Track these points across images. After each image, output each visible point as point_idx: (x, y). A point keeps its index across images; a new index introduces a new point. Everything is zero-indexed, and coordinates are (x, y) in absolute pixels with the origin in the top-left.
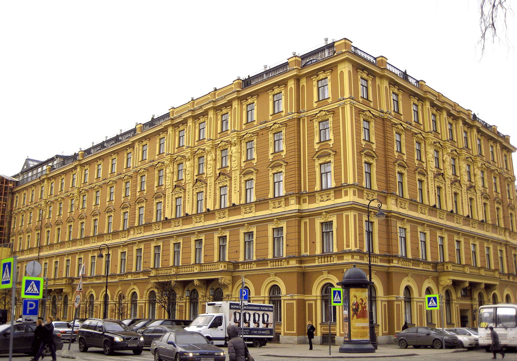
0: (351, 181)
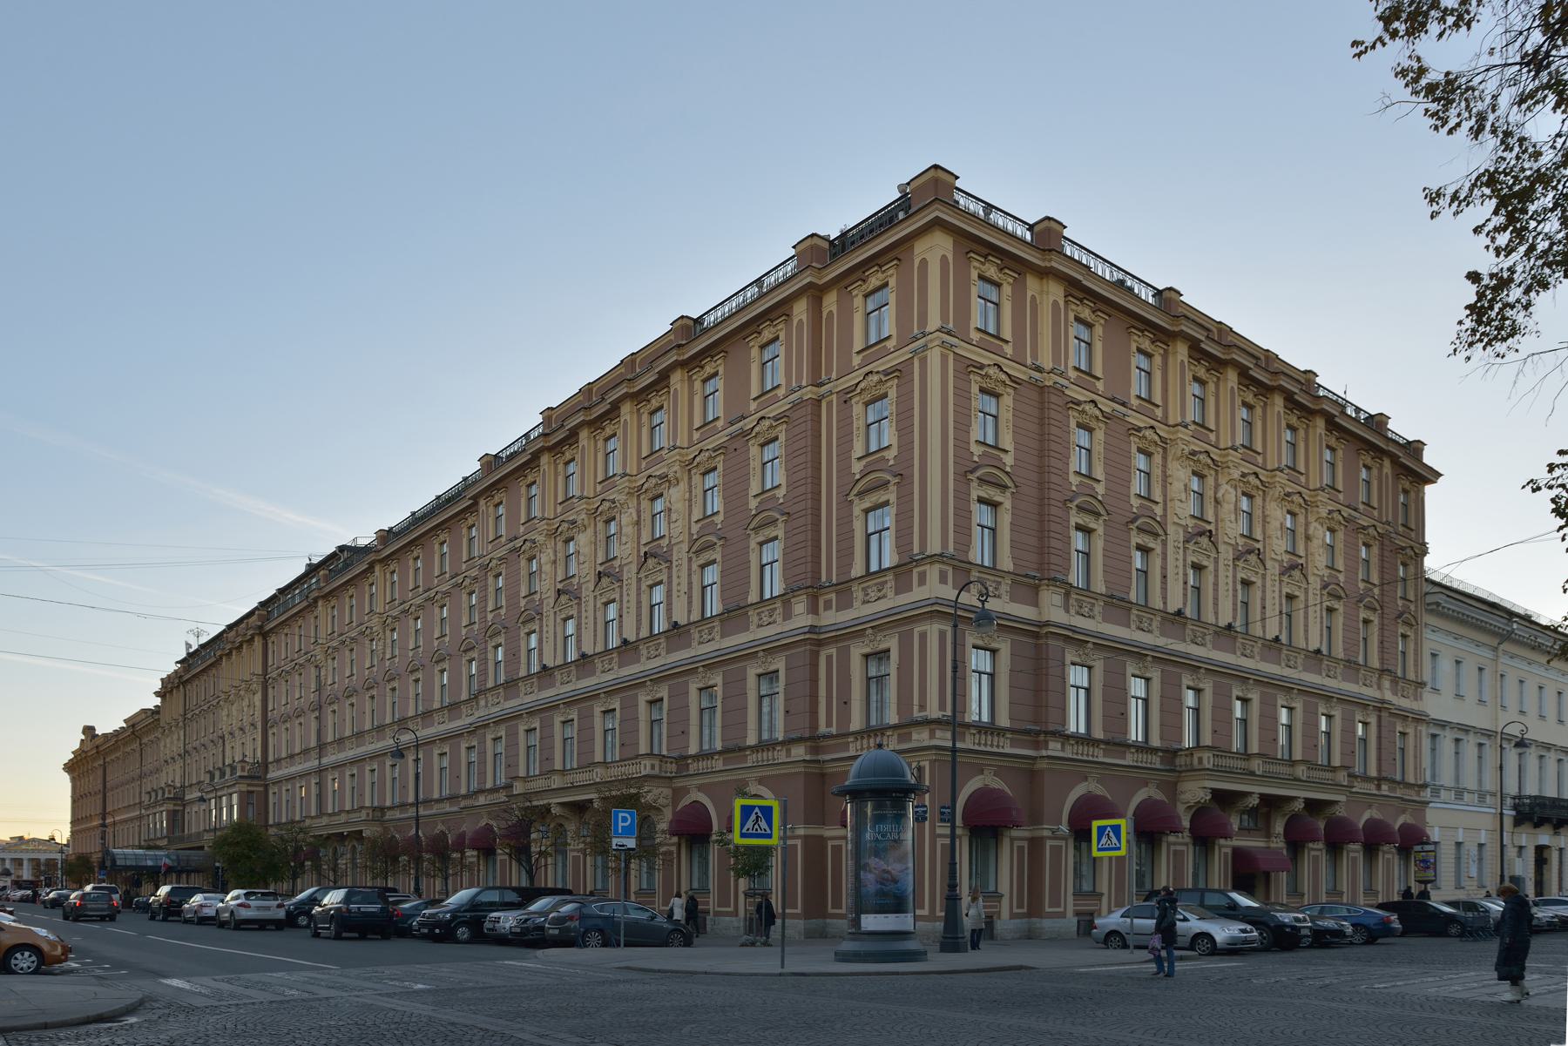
0: (934, 547)
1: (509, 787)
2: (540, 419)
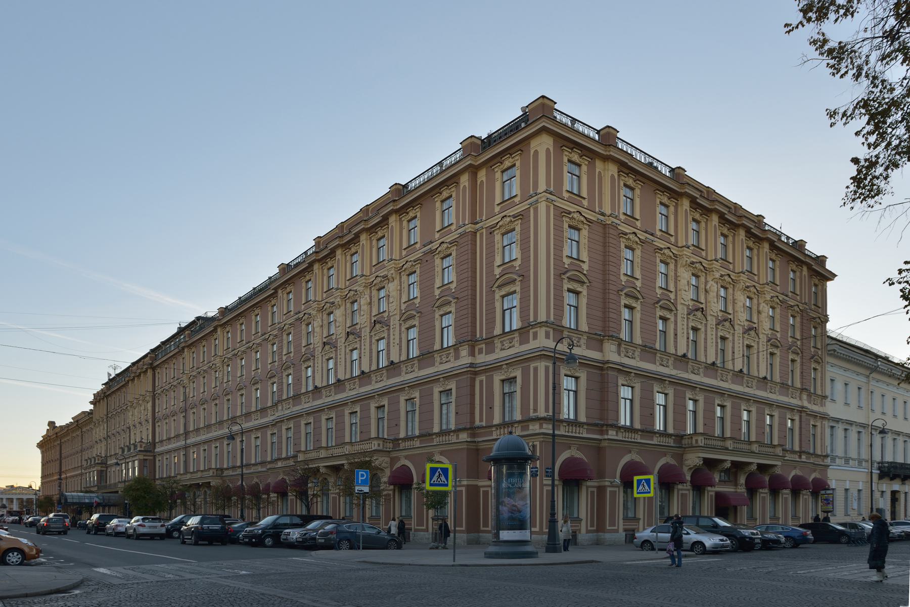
0: (542, 317)
1: (295, 457)
2: (313, 243)
